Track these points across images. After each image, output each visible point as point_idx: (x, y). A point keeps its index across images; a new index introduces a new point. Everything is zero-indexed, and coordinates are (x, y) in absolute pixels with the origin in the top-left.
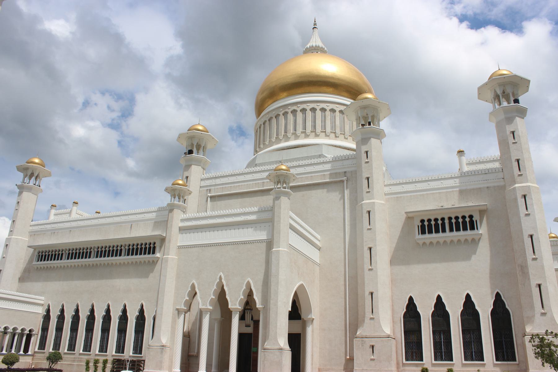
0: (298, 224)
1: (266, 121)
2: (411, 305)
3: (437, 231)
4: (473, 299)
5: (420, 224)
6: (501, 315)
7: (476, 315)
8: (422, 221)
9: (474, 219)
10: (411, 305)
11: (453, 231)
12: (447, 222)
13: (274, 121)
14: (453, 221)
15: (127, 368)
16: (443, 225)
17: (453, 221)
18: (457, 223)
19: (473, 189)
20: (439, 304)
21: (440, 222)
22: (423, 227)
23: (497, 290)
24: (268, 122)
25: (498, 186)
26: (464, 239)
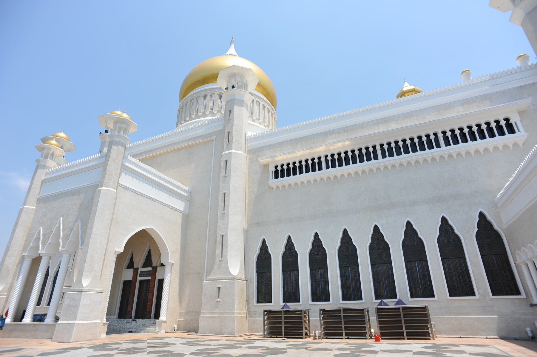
0: (171, 183)
1: (188, 102)
2: (264, 248)
3: (369, 159)
4: (489, 218)
5: (274, 170)
6: (487, 234)
7: (324, 253)
8: (276, 167)
9: (512, 121)
10: (264, 248)
11: (450, 145)
12: (440, 136)
13: (201, 100)
14: (386, 147)
15: (342, 311)
16: (375, 152)
17: (386, 147)
18: (333, 160)
19: (528, 85)
20: (410, 232)
21: (371, 150)
22: (276, 172)
23: (263, 237)
24: (195, 100)
25: (517, 87)
26: (341, 174)
